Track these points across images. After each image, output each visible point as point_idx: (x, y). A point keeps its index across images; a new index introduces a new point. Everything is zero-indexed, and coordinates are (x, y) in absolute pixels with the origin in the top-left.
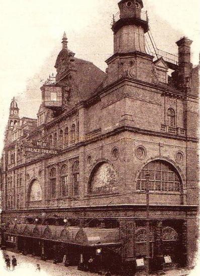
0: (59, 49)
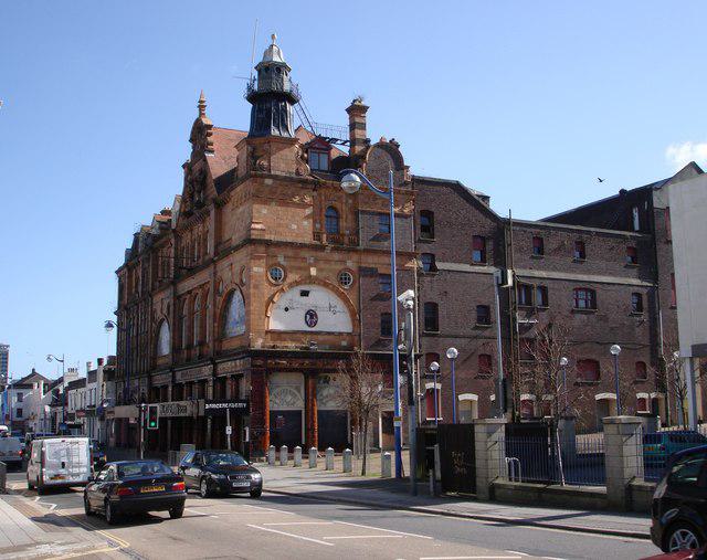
0: (196, 114)
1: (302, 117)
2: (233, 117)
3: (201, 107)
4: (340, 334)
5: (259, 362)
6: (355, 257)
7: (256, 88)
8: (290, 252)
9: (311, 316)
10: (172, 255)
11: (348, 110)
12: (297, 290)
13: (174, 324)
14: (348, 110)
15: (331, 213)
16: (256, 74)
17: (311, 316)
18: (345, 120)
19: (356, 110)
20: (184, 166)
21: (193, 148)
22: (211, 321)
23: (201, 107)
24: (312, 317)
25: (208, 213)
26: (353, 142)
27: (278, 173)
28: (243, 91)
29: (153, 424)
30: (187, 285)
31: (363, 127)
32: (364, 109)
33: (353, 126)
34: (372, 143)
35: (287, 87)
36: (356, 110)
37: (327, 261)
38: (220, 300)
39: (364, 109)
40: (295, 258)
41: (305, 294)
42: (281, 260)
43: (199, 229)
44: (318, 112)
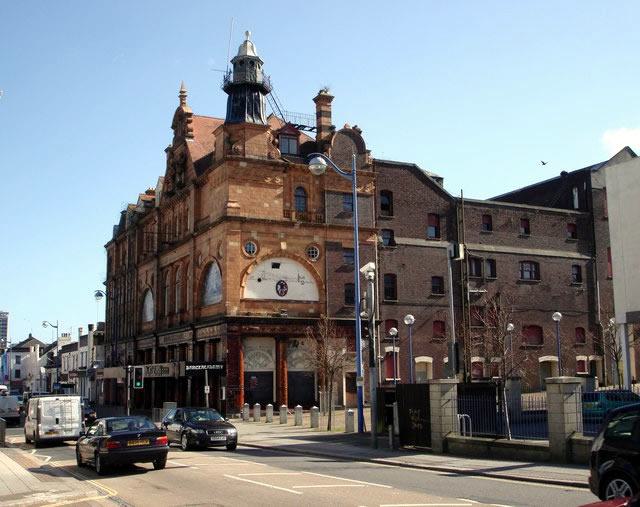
0: (177, 104)
1: (274, 106)
2: (211, 106)
3: (182, 97)
4: (308, 302)
5: (235, 328)
6: (321, 233)
7: (232, 79)
8: (263, 229)
9: (282, 286)
10: (156, 231)
11: (315, 100)
12: (268, 264)
13: (157, 293)
14: (315, 100)
15: (300, 193)
16: (231, 66)
17: (282, 286)
18: (312, 108)
19: (323, 100)
20: (166, 151)
21: (175, 134)
22: (191, 291)
23: (182, 97)
24: (282, 287)
25: (188, 193)
26: (320, 129)
27: (252, 157)
28: (220, 83)
29: (138, 384)
30: (169, 258)
31: (329, 115)
32: (330, 99)
33: (319, 114)
34: (337, 130)
35: (259, 79)
36: (323, 100)
37: (297, 236)
38: (199, 271)
39: (330, 99)
40: (267, 233)
41: (276, 266)
42: (254, 235)
43: (180, 208)
44: (288, 102)
